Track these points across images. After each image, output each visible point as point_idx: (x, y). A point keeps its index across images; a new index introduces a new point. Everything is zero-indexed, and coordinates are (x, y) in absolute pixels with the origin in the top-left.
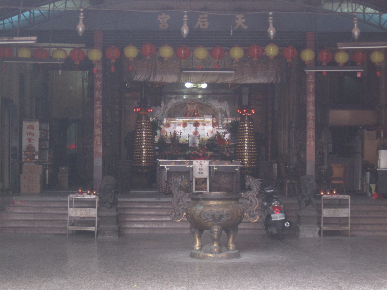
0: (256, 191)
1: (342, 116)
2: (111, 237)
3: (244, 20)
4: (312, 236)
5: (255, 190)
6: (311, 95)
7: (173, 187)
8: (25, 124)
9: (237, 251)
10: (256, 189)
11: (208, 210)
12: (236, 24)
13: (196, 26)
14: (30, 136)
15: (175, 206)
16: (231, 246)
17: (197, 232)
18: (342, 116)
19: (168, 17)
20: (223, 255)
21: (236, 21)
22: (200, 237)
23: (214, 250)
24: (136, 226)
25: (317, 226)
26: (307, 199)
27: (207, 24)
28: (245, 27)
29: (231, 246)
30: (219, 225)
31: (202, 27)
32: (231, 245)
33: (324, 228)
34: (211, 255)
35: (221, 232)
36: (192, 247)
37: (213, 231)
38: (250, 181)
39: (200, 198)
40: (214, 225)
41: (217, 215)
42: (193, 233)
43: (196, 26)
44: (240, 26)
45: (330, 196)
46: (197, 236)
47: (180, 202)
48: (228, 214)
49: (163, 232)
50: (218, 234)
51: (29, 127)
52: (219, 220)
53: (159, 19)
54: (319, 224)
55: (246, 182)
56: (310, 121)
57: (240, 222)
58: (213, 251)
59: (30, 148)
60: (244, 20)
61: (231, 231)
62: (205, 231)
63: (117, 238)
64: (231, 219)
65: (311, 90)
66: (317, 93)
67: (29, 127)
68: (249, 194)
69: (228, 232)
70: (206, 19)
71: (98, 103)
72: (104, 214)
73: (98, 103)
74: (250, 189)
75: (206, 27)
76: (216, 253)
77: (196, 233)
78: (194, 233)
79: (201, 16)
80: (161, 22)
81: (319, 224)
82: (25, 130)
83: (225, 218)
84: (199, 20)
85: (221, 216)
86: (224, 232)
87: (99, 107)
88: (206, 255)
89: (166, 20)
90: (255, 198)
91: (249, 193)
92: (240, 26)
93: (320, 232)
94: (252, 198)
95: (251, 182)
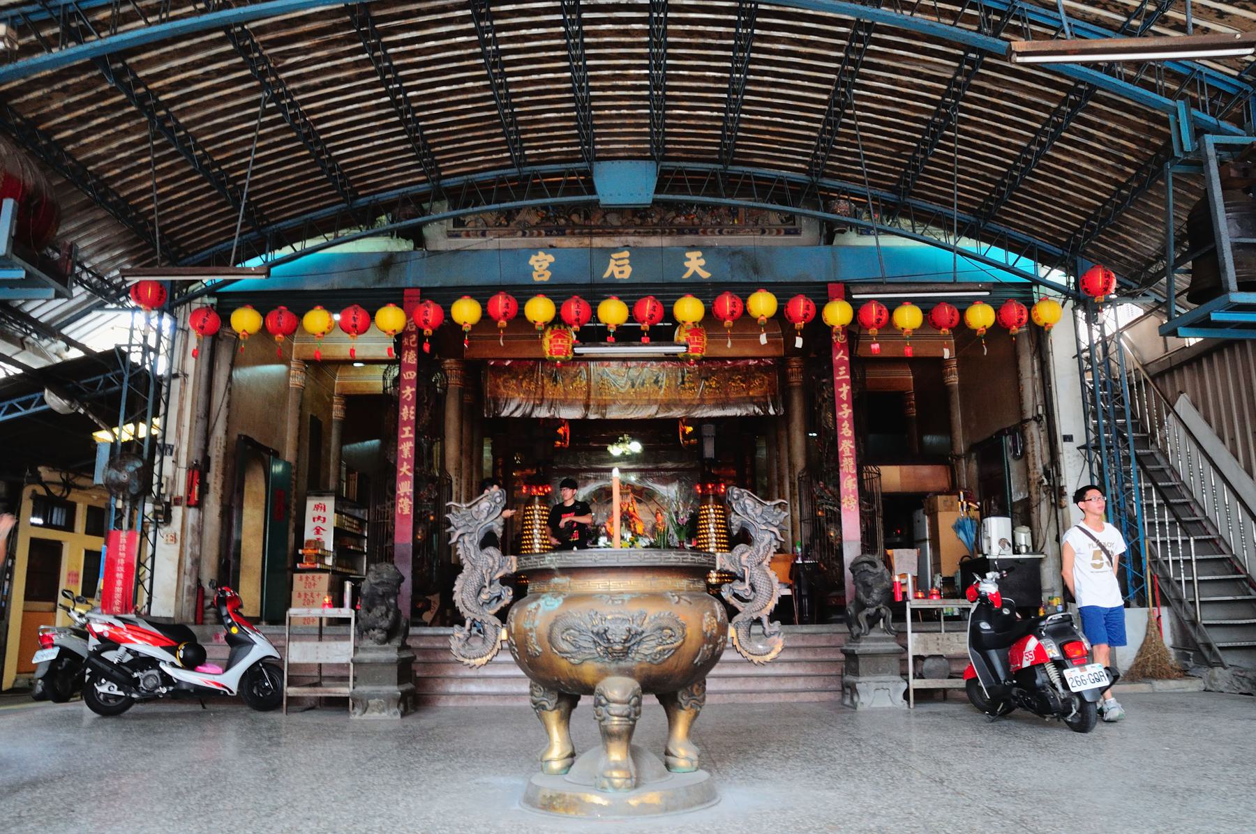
0: (770, 543)
1: (892, 476)
2: (384, 714)
3: (702, 262)
4: (889, 704)
5: (767, 541)
6: (845, 406)
7: (458, 532)
8: (311, 503)
9: (703, 775)
10: (768, 537)
11: (580, 614)
12: (687, 269)
13: (607, 275)
14: (319, 523)
15: (469, 605)
16: (684, 753)
17: (550, 701)
18: (892, 476)
19: (551, 258)
20: (651, 796)
21: (687, 264)
22: (566, 718)
23: (609, 778)
24: (472, 688)
25: (899, 678)
26: (872, 611)
27: (628, 270)
28: (705, 275)
29: (684, 753)
30: (629, 673)
31: (617, 276)
32: (681, 752)
33: (916, 684)
34: (597, 799)
35: (639, 704)
36: (533, 756)
37: (604, 701)
38: (744, 510)
39: (553, 567)
40: (604, 673)
41: (618, 633)
42: (539, 707)
43: (607, 275)
44: (695, 272)
45: (926, 601)
46: (553, 718)
47: (487, 590)
48: (662, 629)
49: (492, 702)
50: (625, 713)
51: (317, 507)
52: (626, 652)
53: (531, 262)
54: (904, 674)
55: (733, 515)
56: (845, 460)
57: (713, 659)
58: (606, 783)
59: (318, 544)
60: (702, 262)
61: (683, 698)
62: (585, 701)
63: (399, 716)
64: (678, 648)
65: (844, 396)
66: (856, 403)
67: (317, 507)
68: (744, 558)
69: (669, 702)
70: (627, 261)
71: (407, 429)
72: (363, 656)
73: (407, 429)
74: (744, 537)
75: (626, 276)
76: (616, 788)
77: (549, 707)
78: (544, 707)
79: (615, 256)
80: (536, 268)
81: (904, 674)
82: (310, 512)
83: (653, 643)
84: (612, 262)
85: (633, 637)
86: (651, 700)
87: (408, 439)
88: (578, 798)
89: (546, 265)
90: (768, 570)
91: (743, 553)
92: (695, 272)
93: (906, 695)
94: (756, 571)
95: (749, 511)
